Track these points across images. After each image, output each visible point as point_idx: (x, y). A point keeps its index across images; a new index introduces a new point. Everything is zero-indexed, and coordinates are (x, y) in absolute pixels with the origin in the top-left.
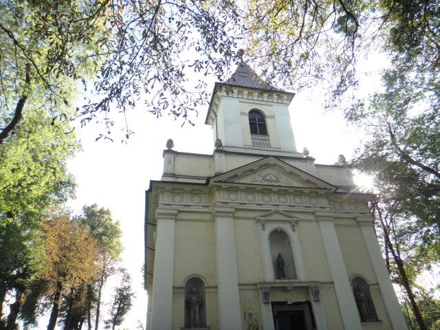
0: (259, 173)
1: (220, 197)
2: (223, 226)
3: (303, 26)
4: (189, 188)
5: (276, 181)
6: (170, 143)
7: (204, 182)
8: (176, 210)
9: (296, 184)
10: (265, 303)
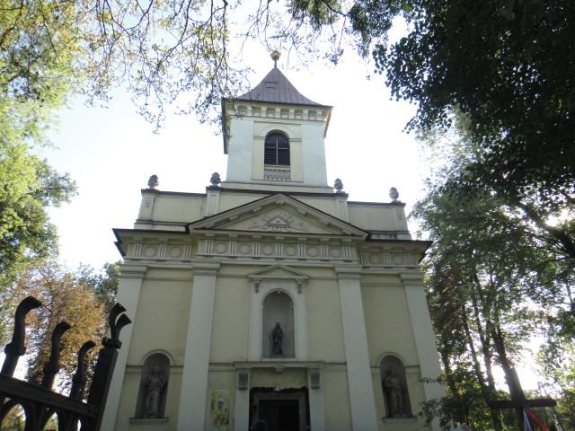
0: (261, 217)
1: (203, 248)
2: (202, 285)
3: (186, 26)
4: (165, 238)
5: (285, 227)
6: (154, 180)
7: (183, 229)
8: (217, 263)
9: (313, 230)
10: (241, 389)
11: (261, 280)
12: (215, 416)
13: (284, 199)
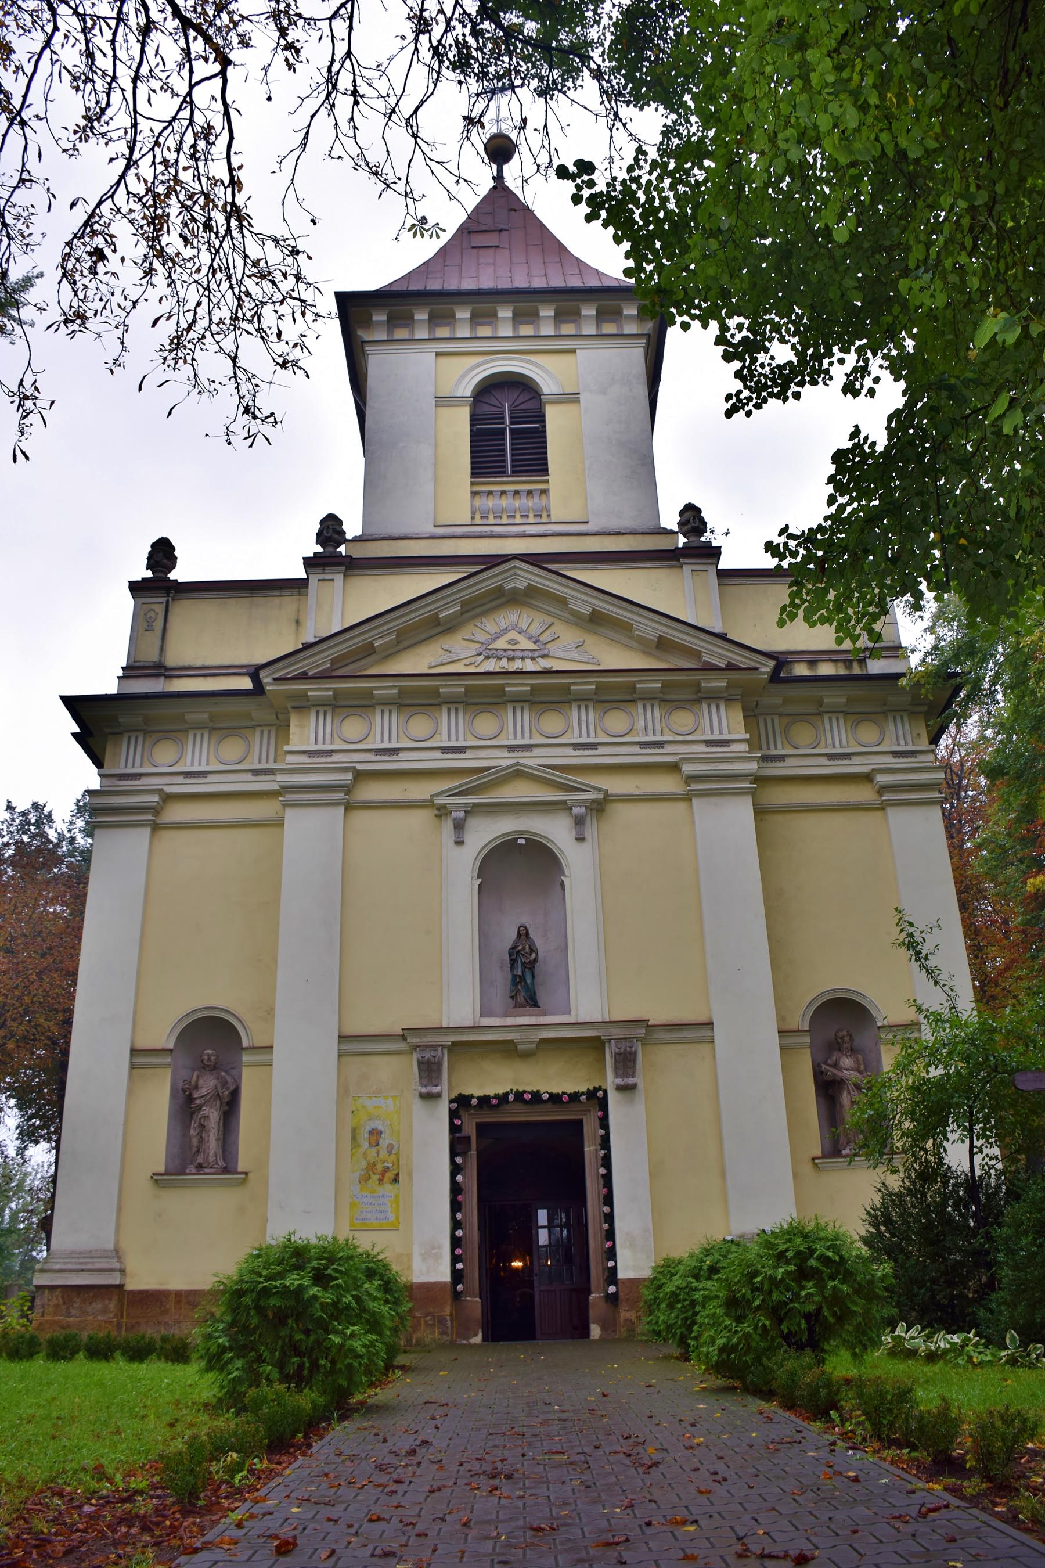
0: (466, 632)
11: (472, 811)
12: (364, 1164)
13: (525, 577)
